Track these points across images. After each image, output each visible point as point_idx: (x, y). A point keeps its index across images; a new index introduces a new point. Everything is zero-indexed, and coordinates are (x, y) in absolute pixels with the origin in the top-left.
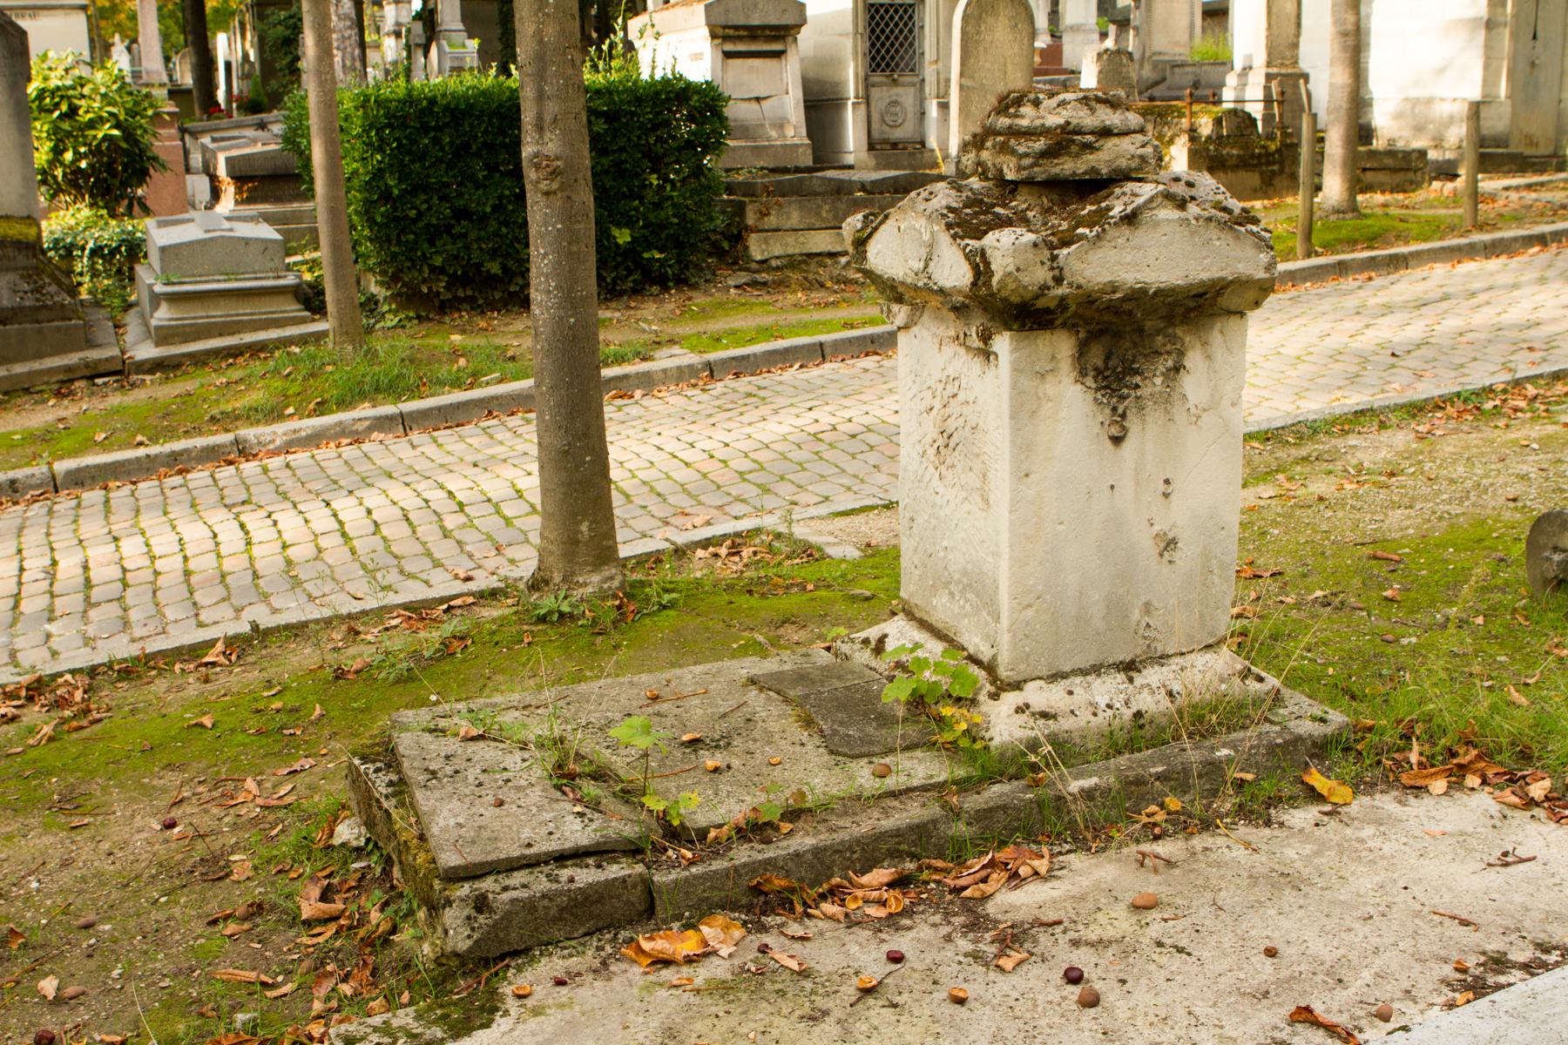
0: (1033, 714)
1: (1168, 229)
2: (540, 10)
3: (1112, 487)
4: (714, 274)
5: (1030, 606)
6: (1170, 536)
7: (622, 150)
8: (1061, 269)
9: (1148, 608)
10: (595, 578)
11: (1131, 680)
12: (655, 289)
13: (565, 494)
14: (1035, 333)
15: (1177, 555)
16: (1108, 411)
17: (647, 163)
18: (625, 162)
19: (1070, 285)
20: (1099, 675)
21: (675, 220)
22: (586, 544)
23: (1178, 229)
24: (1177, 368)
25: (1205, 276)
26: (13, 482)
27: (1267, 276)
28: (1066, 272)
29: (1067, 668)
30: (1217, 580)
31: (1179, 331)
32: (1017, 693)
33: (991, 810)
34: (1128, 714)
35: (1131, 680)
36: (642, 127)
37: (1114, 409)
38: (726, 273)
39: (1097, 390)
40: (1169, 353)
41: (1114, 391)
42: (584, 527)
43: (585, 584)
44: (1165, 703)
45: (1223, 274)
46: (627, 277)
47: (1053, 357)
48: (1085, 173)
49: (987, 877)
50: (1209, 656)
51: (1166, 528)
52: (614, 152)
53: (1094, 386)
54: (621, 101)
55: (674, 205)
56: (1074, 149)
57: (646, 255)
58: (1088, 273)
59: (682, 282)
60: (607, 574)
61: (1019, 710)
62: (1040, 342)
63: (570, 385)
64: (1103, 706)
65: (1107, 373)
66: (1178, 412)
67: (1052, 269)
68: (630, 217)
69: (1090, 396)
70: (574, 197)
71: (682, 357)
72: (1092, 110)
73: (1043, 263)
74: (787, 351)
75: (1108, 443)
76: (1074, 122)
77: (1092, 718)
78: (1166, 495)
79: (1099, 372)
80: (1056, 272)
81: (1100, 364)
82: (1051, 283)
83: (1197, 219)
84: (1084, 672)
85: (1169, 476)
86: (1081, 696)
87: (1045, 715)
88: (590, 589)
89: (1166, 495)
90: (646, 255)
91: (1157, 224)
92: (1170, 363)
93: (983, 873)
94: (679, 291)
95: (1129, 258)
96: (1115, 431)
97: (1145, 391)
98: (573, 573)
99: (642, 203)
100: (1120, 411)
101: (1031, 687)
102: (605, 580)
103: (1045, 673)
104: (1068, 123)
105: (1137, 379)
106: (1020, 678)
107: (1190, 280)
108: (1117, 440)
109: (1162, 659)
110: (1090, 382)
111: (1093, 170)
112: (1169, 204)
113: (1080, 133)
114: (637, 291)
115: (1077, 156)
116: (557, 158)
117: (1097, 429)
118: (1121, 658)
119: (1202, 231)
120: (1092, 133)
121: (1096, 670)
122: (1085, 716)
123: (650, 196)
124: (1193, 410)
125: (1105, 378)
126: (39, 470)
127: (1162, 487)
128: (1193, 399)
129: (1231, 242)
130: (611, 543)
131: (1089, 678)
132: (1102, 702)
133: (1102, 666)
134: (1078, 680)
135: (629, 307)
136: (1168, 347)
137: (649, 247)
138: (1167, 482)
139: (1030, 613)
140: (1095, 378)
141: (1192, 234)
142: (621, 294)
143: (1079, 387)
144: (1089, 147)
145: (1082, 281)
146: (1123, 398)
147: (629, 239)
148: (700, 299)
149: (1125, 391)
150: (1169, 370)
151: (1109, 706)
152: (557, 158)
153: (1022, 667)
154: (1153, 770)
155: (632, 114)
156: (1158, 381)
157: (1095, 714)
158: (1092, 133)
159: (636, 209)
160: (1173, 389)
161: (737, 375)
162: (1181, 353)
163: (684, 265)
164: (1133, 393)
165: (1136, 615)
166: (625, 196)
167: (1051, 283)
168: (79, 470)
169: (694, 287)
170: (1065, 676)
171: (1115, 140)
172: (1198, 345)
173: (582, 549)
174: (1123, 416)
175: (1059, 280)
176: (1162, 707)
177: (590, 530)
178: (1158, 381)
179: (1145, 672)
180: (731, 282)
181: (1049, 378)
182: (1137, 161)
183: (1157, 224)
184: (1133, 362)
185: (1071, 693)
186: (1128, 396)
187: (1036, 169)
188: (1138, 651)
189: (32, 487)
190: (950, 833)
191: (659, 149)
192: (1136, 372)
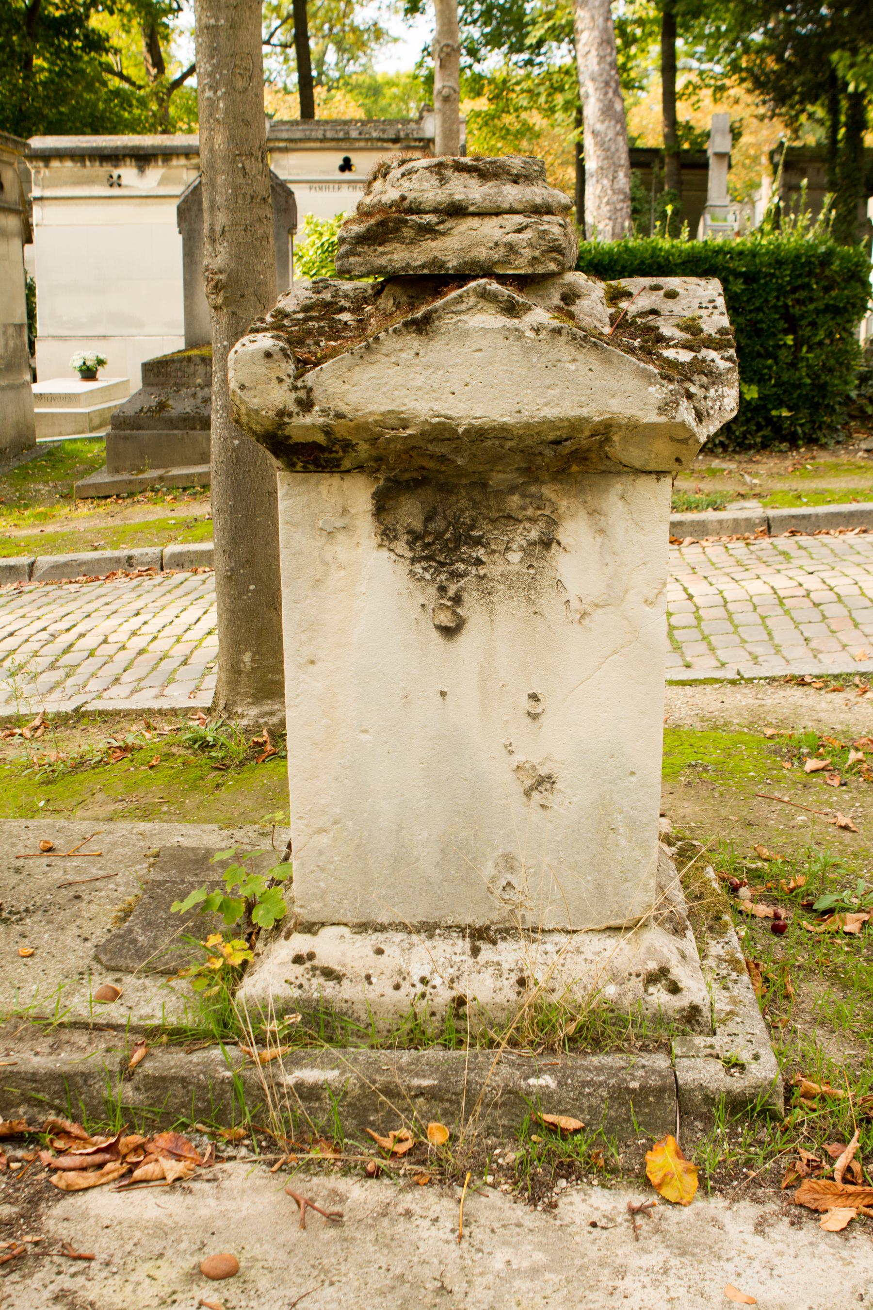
0: (314, 968)
1: (484, 343)
2: (211, 115)
3: (443, 694)
4: (850, 436)
5: (322, 831)
6: (543, 771)
7: (759, 309)
8: (310, 390)
9: (509, 862)
10: (254, 711)
11: (475, 952)
12: (784, 446)
13: (229, 620)
14: (316, 476)
15: (552, 799)
16: (432, 590)
17: (782, 325)
18: (761, 321)
19: (324, 412)
20: (431, 937)
21: (808, 381)
22: (248, 675)
23: (501, 342)
24: (547, 543)
25: (551, 413)
26: (130, 558)
27: (663, 419)
28: (317, 394)
29: (384, 918)
30: (623, 842)
31: (547, 491)
32: (308, 936)
33: (163, 1079)
34: (444, 996)
35: (475, 952)
36: (780, 288)
37: (442, 589)
38: (861, 436)
39: (413, 560)
40: (532, 520)
41: (442, 564)
42: (247, 657)
43: (242, 716)
44: (508, 993)
45: (585, 412)
46: (757, 431)
47: (345, 511)
48: (423, 266)
49: (100, 1166)
50: (611, 943)
51: (535, 760)
52: (751, 311)
53: (409, 554)
54: (761, 263)
55: (809, 367)
56: (407, 232)
57: (774, 413)
58: (354, 397)
59: (812, 441)
60: (266, 708)
61: (298, 960)
62: (323, 489)
63: (234, 510)
64: (416, 979)
65: (429, 539)
66: (549, 602)
67: (295, 388)
68: (762, 375)
69: (403, 568)
70: (240, 313)
71: (753, 510)
72: (443, 180)
73: (280, 380)
74: (852, 515)
75: (436, 635)
76: (411, 196)
77: (390, 992)
78: (534, 716)
79: (415, 538)
80: (302, 394)
81: (417, 525)
82: (293, 408)
83: (537, 331)
84: (402, 927)
85: (537, 691)
86: (393, 957)
87: (329, 974)
88: (245, 722)
89: (534, 716)
90: (774, 413)
91: (465, 334)
92: (534, 535)
93: (99, 1158)
94: (809, 450)
95: (419, 381)
96: (445, 619)
97: (494, 568)
98: (235, 703)
99: (776, 363)
100: (451, 593)
101: (328, 932)
102: (263, 715)
103: (351, 918)
104: (403, 198)
105: (480, 552)
106: (314, 919)
107: (525, 417)
108: (449, 632)
109: (534, 932)
110: (401, 547)
111: (435, 262)
112: (491, 308)
113: (419, 211)
114: (764, 446)
115: (412, 242)
116: (221, 272)
117: (417, 612)
118: (468, 920)
119: (544, 347)
120: (435, 211)
121: (429, 929)
122: (382, 986)
123: (784, 356)
124: (575, 604)
125: (427, 546)
126: (152, 551)
127: (526, 704)
128: (573, 589)
129: (596, 365)
130: (277, 677)
131: (415, 938)
132: (417, 971)
133: (436, 925)
134: (399, 937)
135: (750, 461)
136: (530, 512)
137: (780, 404)
138: (534, 697)
139: (324, 840)
140: (411, 545)
141: (527, 351)
142: (750, 447)
143: (385, 554)
144: (428, 230)
145: (343, 408)
146: (456, 575)
147: (756, 396)
148: (824, 458)
149: (461, 566)
150: (532, 544)
151: (424, 981)
152: (221, 272)
153: (317, 906)
154: (416, 1082)
155: (772, 275)
156: (515, 557)
157: (397, 987)
158: (435, 211)
159: (770, 368)
160: (540, 571)
161: (793, 533)
162: (553, 523)
163: (816, 425)
164: (473, 570)
165: (489, 869)
166: (759, 355)
167: (293, 408)
168: (181, 554)
169: (823, 447)
170: (381, 928)
171: (474, 222)
172: (582, 514)
173: (244, 678)
174: (457, 600)
175: (306, 405)
176: (500, 998)
177: (253, 660)
178: (515, 557)
179: (501, 945)
180: (863, 446)
181: (341, 537)
182: (502, 250)
183: (465, 334)
184: (472, 527)
185: (380, 952)
186: (466, 574)
187: (352, 259)
188: (495, 917)
189: (143, 564)
190: (105, 1093)
191: (797, 311)
192: (478, 542)
